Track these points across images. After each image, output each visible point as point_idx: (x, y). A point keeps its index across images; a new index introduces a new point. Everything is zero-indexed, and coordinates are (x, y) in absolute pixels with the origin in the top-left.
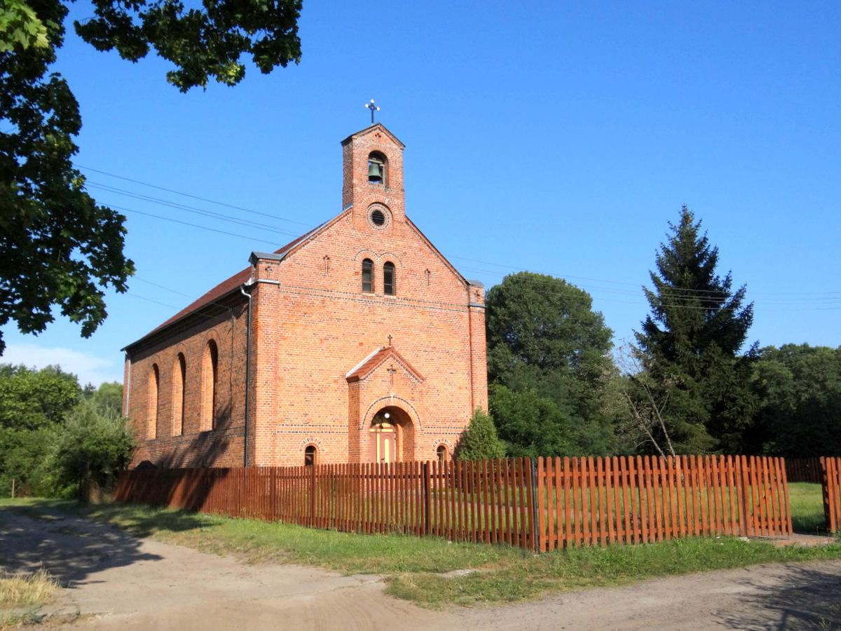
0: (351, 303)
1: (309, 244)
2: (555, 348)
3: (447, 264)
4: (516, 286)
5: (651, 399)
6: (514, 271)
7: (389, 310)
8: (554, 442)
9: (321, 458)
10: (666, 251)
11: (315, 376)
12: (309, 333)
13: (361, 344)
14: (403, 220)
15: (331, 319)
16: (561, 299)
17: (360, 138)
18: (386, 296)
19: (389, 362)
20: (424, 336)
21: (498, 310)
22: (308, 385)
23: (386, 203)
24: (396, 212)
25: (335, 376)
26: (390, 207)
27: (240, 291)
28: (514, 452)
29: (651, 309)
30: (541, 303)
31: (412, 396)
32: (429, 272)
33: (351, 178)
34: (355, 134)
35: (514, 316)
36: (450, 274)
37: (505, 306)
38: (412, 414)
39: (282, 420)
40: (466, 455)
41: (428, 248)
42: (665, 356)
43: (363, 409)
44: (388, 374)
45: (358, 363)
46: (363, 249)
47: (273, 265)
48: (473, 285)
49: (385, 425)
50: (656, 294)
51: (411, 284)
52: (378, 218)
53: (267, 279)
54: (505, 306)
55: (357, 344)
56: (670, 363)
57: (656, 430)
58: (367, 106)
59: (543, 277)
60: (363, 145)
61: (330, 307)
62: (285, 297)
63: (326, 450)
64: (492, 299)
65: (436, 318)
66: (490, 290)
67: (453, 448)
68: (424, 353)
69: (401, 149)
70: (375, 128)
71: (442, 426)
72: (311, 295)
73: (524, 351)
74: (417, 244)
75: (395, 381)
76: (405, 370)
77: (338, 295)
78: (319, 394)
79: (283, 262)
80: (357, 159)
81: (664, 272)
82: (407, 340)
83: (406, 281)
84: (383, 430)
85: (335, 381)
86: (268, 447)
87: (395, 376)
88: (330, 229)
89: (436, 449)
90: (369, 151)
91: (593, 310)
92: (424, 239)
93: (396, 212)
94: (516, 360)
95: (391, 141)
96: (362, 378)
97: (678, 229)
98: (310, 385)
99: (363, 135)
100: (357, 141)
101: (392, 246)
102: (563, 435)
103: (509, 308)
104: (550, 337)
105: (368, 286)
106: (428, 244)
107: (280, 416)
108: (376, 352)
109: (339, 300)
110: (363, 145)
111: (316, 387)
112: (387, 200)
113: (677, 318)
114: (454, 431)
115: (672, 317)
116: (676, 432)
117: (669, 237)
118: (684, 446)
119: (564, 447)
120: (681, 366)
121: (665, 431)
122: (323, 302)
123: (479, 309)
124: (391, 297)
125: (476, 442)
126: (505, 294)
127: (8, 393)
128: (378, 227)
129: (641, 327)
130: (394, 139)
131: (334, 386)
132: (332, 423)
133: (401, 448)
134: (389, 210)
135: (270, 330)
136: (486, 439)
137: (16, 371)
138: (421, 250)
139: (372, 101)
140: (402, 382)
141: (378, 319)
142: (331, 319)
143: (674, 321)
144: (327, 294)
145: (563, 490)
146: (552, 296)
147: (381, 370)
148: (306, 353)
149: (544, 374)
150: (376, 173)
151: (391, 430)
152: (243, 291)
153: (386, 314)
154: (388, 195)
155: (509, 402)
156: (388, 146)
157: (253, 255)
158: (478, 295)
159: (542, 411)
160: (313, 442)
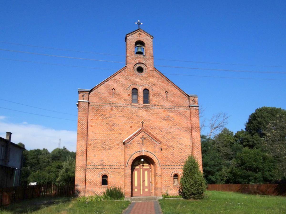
0: (126, 109)
1: (105, 84)
4: (260, 112)
6: (260, 106)
7: (146, 111)
9: (110, 180)
11: (107, 143)
12: (104, 123)
13: (131, 127)
14: (153, 69)
15: (115, 116)
17: (130, 36)
18: (144, 104)
19: (141, 135)
20: (165, 122)
21: (253, 122)
22: (103, 147)
23: (144, 63)
25: (118, 142)
26: (146, 64)
28: (251, 175)
31: (155, 150)
32: (168, 92)
35: (259, 123)
36: (179, 92)
37: (256, 120)
38: (155, 159)
39: (90, 163)
41: (167, 81)
44: (141, 140)
46: (132, 84)
47: (86, 94)
48: (191, 97)
52: (140, 70)
53: (83, 99)
54: (256, 120)
55: (129, 127)
58: (136, 23)
59: (272, 108)
61: (115, 111)
62: (92, 108)
63: (112, 176)
65: (172, 113)
66: (251, 115)
68: (165, 130)
69: (152, 38)
70: (138, 31)
71: (176, 164)
72: (105, 106)
76: (150, 138)
77: (119, 105)
78: (109, 151)
79: (92, 93)
82: (156, 124)
84: (144, 167)
85: (118, 145)
86: (81, 176)
87: (145, 141)
88: (115, 76)
89: (172, 176)
90: (135, 41)
92: (164, 77)
93: (149, 66)
95: (146, 36)
98: (104, 147)
99: (132, 34)
100: (129, 37)
101: (147, 81)
103: (258, 121)
106: (167, 79)
109: (120, 108)
110: (133, 39)
122: (112, 109)
123: (195, 107)
124: (147, 105)
128: (140, 74)
130: (148, 34)
132: (115, 164)
134: (146, 66)
135: (84, 122)
138: (163, 82)
139: (139, 21)
140: (149, 144)
142: (115, 116)
144: (114, 105)
147: (138, 139)
148: (103, 132)
150: (140, 50)
151: (148, 167)
153: (144, 113)
155: (248, 154)
156: (145, 38)
158: (195, 101)
160: (106, 173)
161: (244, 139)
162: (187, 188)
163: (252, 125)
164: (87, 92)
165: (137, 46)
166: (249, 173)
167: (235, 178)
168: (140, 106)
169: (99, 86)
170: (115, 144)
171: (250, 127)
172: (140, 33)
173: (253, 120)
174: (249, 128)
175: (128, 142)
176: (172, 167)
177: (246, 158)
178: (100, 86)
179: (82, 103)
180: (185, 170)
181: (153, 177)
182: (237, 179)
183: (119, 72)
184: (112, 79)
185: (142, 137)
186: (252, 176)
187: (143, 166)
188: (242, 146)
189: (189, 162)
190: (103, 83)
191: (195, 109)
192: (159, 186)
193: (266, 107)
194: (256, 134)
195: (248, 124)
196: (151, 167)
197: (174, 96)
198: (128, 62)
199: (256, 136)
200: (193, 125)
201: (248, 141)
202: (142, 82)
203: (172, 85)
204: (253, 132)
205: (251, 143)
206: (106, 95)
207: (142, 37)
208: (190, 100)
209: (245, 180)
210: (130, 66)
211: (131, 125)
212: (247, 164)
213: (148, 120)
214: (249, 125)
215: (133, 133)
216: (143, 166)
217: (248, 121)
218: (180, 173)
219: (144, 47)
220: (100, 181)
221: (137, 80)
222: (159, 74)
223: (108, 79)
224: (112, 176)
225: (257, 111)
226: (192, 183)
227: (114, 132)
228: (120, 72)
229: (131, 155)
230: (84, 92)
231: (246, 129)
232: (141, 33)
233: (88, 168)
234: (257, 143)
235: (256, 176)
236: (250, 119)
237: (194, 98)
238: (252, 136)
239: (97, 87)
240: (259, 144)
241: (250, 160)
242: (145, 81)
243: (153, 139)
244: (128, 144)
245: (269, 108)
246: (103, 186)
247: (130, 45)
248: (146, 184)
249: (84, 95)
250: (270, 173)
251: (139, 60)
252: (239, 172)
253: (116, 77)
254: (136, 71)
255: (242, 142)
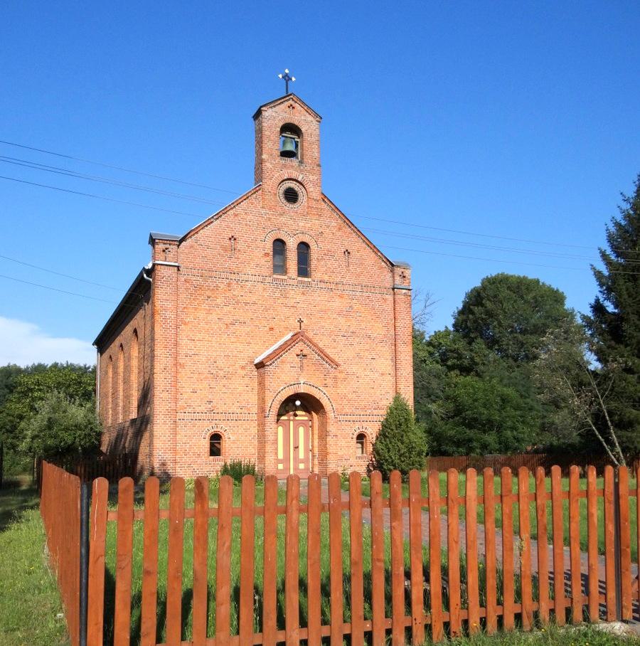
2: (527, 342)
3: (369, 244)
4: (493, 287)
5: (594, 383)
6: (493, 272)
7: (303, 294)
8: (513, 428)
10: (617, 224)
11: (220, 363)
12: (214, 317)
13: (271, 329)
14: (319, 197)
15: (238, 302)
16: (534, 298)
17: (270, 110)
18: (300, 279)
19: (296, 349)
20: (342, 320)
21: (476, 309)
23: (299, 180)
24: (310, 188)
25: (243, 363)
26: (305, 183)
27: (143, 276)
29: (598, 288)
30: (515, 301)
31: (325, 382)
32: (349, 253)
33: (261, 154)
34: (264, 106)
35: (490, 314)
36: (373, 255)
37: (482, 305)
38: (324, 402)
40: (382, 443)
42: (612, 339)
43: (269, 397)
44: (298, 359)
45: (267, 348)
47: (172, 246)
49: (298, 413)
50: (606, 273)
51: (329, 266)
52: (291, 196)
53: (165, 261)
54: (482, 305)
55: (267, 329)
56: (617, 346)
57: (598, 417)
58: (280, 76)
59: (519, 277)
60: (275, 117)
63: (233, 438)
64: (470, 299)
67: (374, 436)
70: (288, 98)
73: (499, 346)
74: (335, 222)
75: (305, 365)
78: (224, 381)
79: (184, 243)
80: (266, 133)
81: (615, 248)
82: (323, 324)
83: (322, 263)
84: (297, 418)
85: (243, 368)
87: (305, 361)
89: (355, 437)
90: (281, 124)
91: (566, 307)
93: (311, 189)
94: (493, 355)
95: (306, 113)
96: (268, 363)
97: (631, 201)
99: (274, 106)
100: (267, 113)
101: (307, 225)
102: (523, 422)
103: (486, 307)
104: (523, 332)
105: (280, 268)
107: (180, 403)
108: (288, 337)
109: (247, 283)
110: (275, 117)
111: (221, 373)
112: (301, 176)
113: (626, 297)
114: (375, 418)
115: (620, 297)
116: (621, 421)
117: (621, 209)
118: (629, 434)
119: (524, 433)
120: (628, 348)
121: (608, 418)
122: (229, 285)
123: (404, 291)
124: (306, 279)
125: (392, 430)
126: (483, 295)
127: (38, 386)
128: (291, 206)
129: (590, 309)
130: (310, 110)
131: (243, 372)
132: (239, 411)
133: (316, 437)
134: (302, 185)
135: (168, 314)
136: (403, 427)
137: (90, 370)
138: (340, 229)
139: (287, 71)
141: (291, 302)
142: (238, 302)
143: (622, 300)
144: (233, 277)
145: (515, 480)
146: (526, 294)
147: (290, 356)
148: (210, 339)
149: (518, 367)
150: (290, 147)
151: (306, 418)
152: (145, 276)
153: (299, 298)
154: (301, 171)
155: (471, 391)
156: (303, 118)
157: (151, 236)
158: (404, 277)
159: (503, 400)
161: (451, 351)
162: (392, 461)
163: (471, 316)
164: (173, 243)
165: (283, 136)
166: (470, 433)
167: (440, 445)
168: (291, 282)
169: (199, 229)
170: (237, 366)
171: (467, 322)
172: (291, 105)
173: (474, 305)
174: (464, 323)
175: (271, 364)
176: (354, 418)
177: (466, 400)
178: (202, 228)
179: (162, 267)
180: (386, 426)
181: (317, 440)
182: (444, 448)
183: (245, 197)
184: (228, 213)
185: (299, 353)
186: (477, 440)
187: (296, 415)
188: (444, 368)
189: (396, 409)
190: (209, 222)
191: (405, 294)
192: (331, 458)
193: (507, 275)
194: (479, 340)
195: (461, 312)
196: (312, 418)
197: (362, 264)
198: (266, 175)
199: (479, 344)
200: (398, 329)
201: (460, 357)
202: (296, 225)
203: (359, 236)
204: (472, 335)
205: (466, 362)
206: (215, 252)
207: (297, 115)
208: (394, 274)
209: (461, 449)
210: (270, 183)
211: (272, 324)
212: (467, 413)
213: (308, 314)
214: (465, 317)
215: (276, 343)
216: (296, 415)
217: (460, 306)
218: (372, 431)
219: (298, 140)
220: (206, 446)
221: (283, 219)
222: (332, 209)
223: (221, 214)
224: (233, 438)
225: (487, 283)
226: (402, 452)
227: (235, 340)
228: (248, 198)
229: (277, 392)
230: (168, 242)
231: (454, 326)
232: (294, 106)
233: (180, 420)
234: (481, 362)
235: (487, 441)
236: (468, 302)
237: (403, 270)
238: (470, 343)
239: (196, 231)
240: (484, 364)
241: (476, 403)
242: (301, 224)
243: (322, 357)
244: (271, 367)
245: (512, 276)
246: (212, 457)
247: (269, 134)
248: (301, 455)
249: (166, 249)
250: (515, 433)
251: (289, 171)
252: (451, 431)
253: (238, 209)
254: (282, 197)
255: (444, 360)
